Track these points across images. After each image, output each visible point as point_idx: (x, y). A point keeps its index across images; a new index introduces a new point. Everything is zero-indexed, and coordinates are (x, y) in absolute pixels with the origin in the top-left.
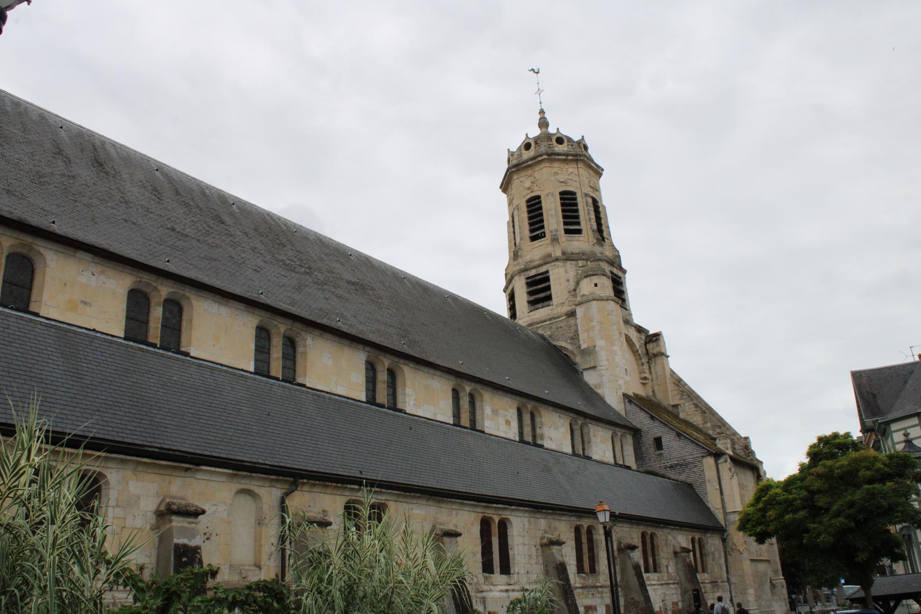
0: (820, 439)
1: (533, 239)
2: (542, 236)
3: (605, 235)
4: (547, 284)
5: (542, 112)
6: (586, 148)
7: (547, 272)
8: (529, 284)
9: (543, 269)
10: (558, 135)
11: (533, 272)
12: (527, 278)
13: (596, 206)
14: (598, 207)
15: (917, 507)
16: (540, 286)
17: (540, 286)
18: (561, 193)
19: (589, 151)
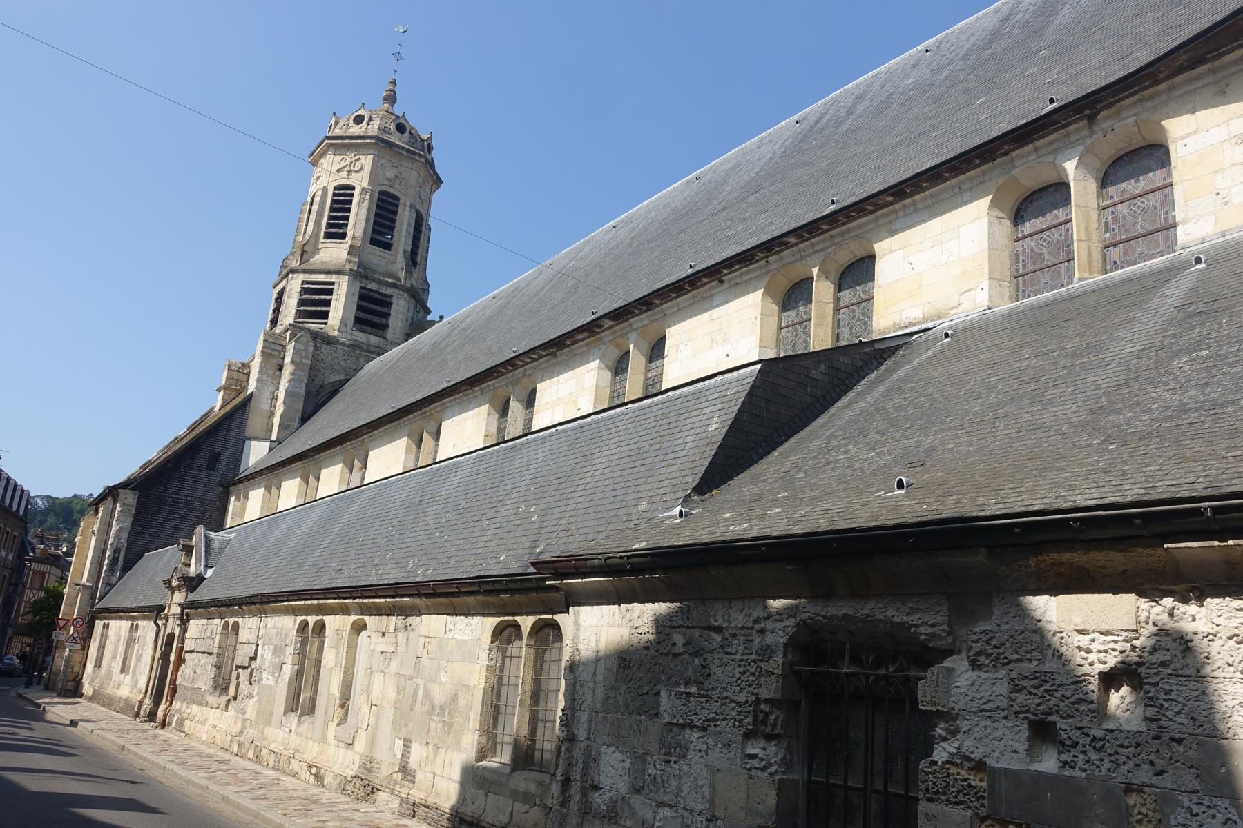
0: (75, 496)
1: (329, 236)
2: (343, 236)
3: (419, 259)
4: (385, 310)
5: (394, 83)
6: (430, 148)
7: (391, 296)
8: (304, 291)
9: (388, 291)
10: (402, 121)
11: (373, 286)
12: (304, 282)
13: (420, 227)
14: (421, 225)
15: (1052, 610)
16: (372, 306)
17: (372, 306)
18: (381, 193)
19: (433, 153)
